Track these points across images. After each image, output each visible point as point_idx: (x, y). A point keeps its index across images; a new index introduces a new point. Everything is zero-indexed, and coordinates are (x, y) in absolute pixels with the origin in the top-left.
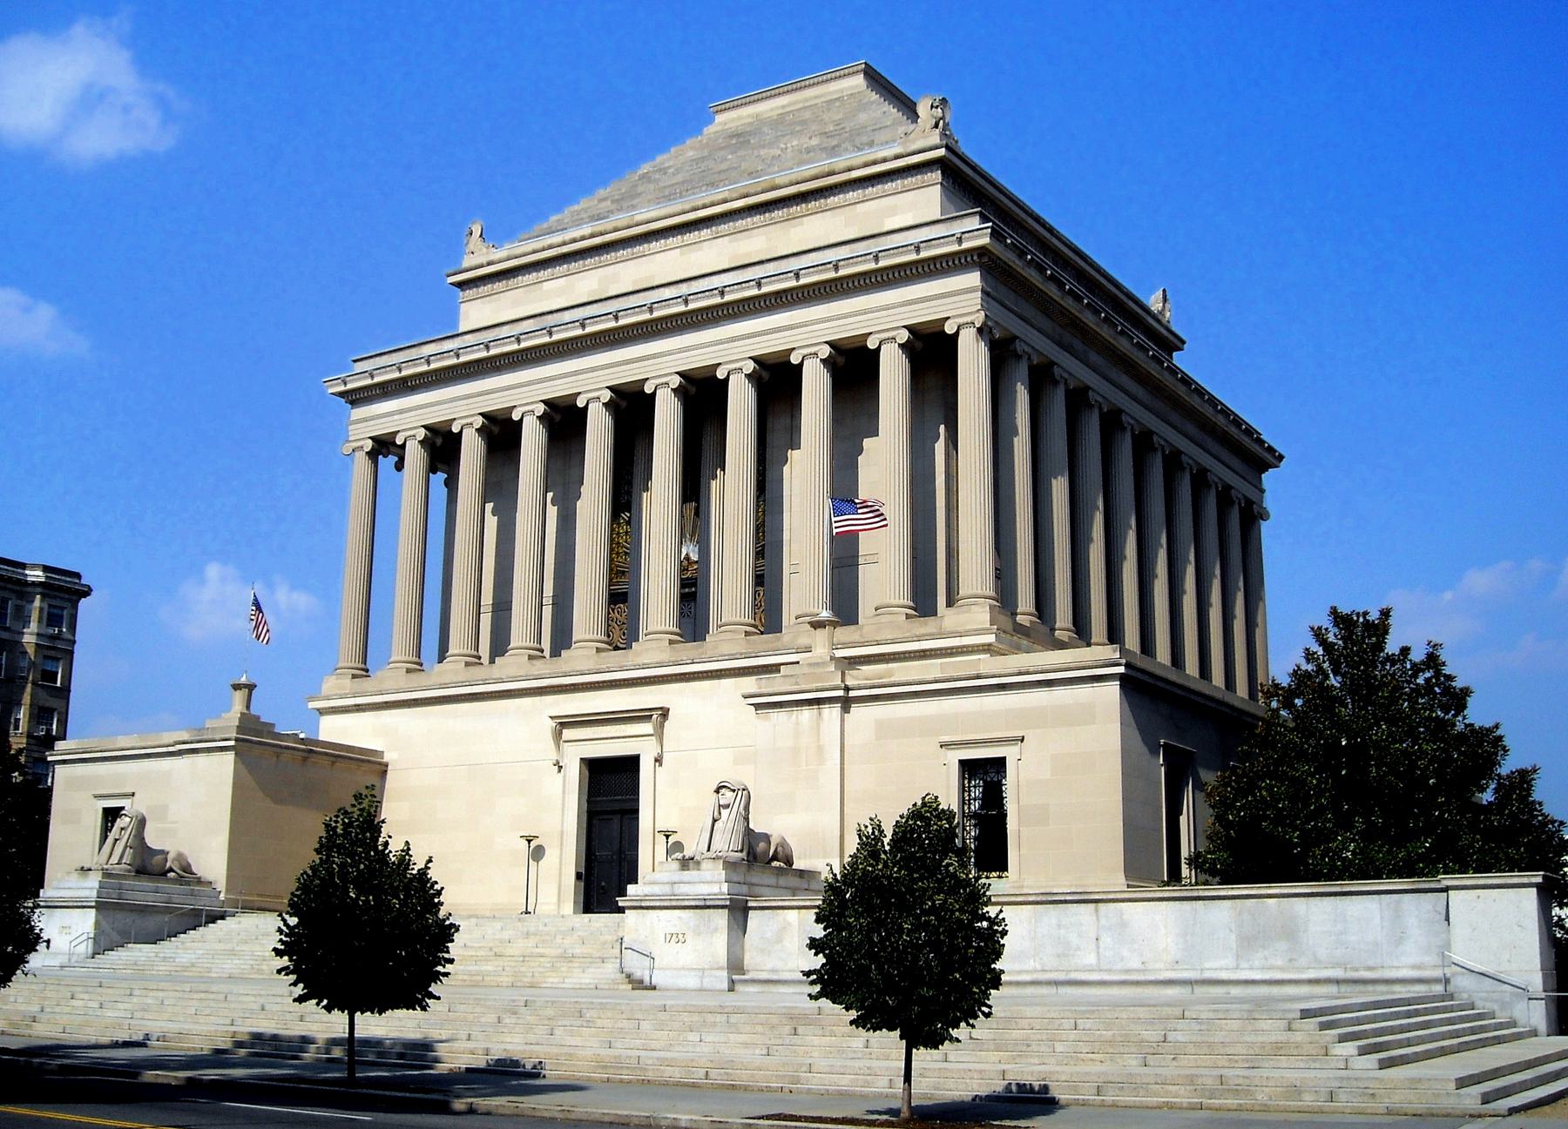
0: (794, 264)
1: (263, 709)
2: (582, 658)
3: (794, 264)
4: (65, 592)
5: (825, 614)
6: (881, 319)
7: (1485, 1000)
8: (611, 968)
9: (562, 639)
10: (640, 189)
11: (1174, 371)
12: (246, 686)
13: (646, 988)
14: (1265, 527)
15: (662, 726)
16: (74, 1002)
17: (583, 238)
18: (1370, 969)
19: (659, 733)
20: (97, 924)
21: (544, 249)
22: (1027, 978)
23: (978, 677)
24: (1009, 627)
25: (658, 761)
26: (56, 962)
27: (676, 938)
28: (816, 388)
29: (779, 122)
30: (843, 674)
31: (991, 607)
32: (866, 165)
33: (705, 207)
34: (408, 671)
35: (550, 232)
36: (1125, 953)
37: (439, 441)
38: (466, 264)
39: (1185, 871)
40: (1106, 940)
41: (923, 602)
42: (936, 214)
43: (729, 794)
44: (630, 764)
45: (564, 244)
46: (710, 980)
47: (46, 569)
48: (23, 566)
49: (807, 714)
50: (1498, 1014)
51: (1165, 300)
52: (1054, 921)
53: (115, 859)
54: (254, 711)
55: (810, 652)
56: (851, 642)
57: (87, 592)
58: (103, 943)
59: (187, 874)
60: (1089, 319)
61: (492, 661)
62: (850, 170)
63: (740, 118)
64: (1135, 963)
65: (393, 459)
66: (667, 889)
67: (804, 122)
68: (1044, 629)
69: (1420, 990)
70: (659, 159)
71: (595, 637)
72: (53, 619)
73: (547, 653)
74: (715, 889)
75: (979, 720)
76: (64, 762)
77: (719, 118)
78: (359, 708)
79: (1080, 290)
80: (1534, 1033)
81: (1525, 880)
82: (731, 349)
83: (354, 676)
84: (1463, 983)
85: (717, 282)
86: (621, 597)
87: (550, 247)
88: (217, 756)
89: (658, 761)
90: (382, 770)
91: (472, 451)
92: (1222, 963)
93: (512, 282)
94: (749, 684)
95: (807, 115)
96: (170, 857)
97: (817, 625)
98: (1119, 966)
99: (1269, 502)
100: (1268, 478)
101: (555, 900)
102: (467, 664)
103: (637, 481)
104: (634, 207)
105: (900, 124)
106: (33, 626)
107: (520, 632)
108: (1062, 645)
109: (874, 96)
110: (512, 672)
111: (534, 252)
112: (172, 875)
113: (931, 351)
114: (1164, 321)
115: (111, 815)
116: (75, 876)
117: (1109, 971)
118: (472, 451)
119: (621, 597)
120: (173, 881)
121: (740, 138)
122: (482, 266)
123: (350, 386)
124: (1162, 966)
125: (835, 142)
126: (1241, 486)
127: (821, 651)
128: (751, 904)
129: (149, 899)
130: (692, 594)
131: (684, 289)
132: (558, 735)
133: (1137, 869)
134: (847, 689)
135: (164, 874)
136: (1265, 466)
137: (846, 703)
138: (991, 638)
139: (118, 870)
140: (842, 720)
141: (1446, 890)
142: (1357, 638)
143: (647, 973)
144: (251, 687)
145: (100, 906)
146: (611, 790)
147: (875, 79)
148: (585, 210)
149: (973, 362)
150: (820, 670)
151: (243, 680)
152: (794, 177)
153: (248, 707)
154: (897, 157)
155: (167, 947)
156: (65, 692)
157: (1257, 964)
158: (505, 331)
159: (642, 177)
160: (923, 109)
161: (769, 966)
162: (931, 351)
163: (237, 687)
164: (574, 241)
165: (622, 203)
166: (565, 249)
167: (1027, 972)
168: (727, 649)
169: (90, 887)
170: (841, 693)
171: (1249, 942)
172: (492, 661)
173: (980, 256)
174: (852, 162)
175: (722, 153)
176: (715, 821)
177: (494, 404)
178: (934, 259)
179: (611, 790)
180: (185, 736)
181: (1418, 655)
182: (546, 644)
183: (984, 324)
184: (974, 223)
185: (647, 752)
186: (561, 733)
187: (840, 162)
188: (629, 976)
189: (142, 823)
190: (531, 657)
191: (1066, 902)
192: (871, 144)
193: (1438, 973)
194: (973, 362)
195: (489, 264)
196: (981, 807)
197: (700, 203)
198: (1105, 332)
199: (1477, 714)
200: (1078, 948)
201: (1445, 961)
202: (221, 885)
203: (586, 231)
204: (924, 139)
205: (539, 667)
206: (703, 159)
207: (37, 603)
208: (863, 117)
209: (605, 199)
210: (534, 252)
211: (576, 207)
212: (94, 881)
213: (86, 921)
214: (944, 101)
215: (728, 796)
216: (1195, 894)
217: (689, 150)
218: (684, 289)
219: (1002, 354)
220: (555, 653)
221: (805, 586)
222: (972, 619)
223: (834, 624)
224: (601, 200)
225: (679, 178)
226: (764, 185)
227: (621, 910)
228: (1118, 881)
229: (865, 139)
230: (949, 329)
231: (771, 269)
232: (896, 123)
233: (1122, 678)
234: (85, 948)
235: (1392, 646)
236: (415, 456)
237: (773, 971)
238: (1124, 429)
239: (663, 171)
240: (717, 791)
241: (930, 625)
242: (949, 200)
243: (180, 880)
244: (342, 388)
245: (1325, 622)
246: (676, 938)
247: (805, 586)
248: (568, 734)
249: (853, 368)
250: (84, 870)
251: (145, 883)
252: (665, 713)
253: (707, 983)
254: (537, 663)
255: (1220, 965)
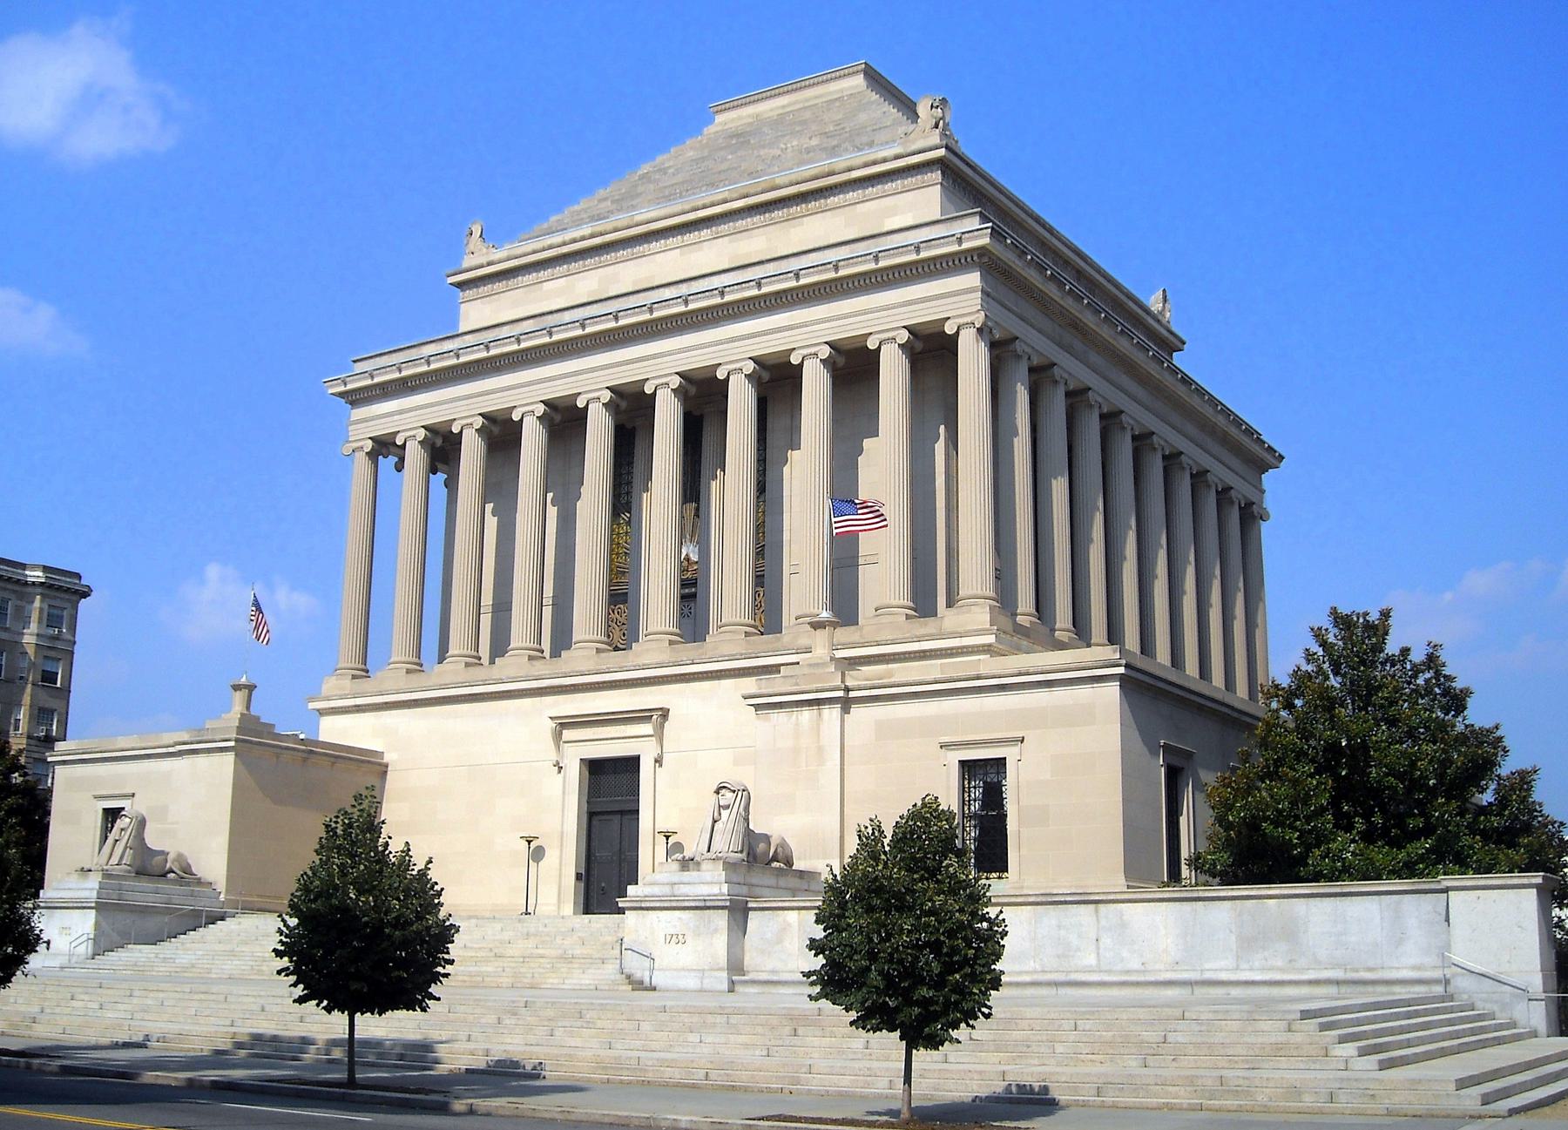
0: (795, 264)
1: (264, 710)
2: (582, 658)
3: (795, 264)
4: (66, 591)
5: (825, 615)
6: (880, 319)
7: (1485, 1001)
8: (611, 969)
9: (562, 640)
10: (640, 189)
11: (1174, 371)
12: (246, 687)
13: (646, 989)
14: (1265, 528)
15: (662, 727)
16: (74, 1003)
17: (583, 239)
18: (1370, 969)
19: (659, 734)
20: (97, 925)
21: (544, 250)
22: (1027, 978)
23: (978, 678)
24: (1010, 628)
25: (658, 761)
26: (56, 963)
27: (676, 938)
28: (815, 387)
29: (779, 121)
30: (843, 675)
31: (991, 607)
32: (866, 165)
33: (705, 207)
34: (408, 671)
35: (550, 232)
36: (1125, 954)
37: (439, 442)
38: (466, 264)
39: (1185, 871)
40: (1106, 941)
41: (923, 602)
42: (939, 217)
43: (730, 795)
44: (630, 765)
45: (564, 244)
46: (714, 980)
47: (46, 569)
48: (23, 566)
49: (806, 715)
50: (1498, 1015)
51: (1165, 300)
52: (1054, 922)
53: (115, 860)
54: (253, 711)
55: (811, 653)
56: (852, 644)
57: (85, 595)
58: (103, 944)
59: (186, 875)
60: (1089, 319)
61: (492, 662)
62: (850, 170)
63: (740, 118)
64: (1135, 964)
65: (393, 460)
66: (667, 890)
67: (804, 123)
68: (1044, 630)
69: (1420, 990)
70: (659, 159)
71: (595, 637)
72: (53, 620)
73: (547, 654)
74: (716, 890)
75: (979, 720)
76: (64, 762)
77: (719, 118)
78: (359, 709)
79: (1081, 289)
80: (1534, 1034)
81: (1525, 881)
82: (731, 350)
83: (354, 677)
84: (1463, 984)
85: (717, 282)
86: (621, 596)
87: (551, 247)
88: (216, 757)
89: (658, 761)
90: (383, 771)
91: (472, 451)
92: (1222, 964)
93: (512, 283)
94: (749, 684)
95: (808, 115)
96: (170, 857)
97: (817, 626)
98: (1119, 967)
99: (1269, 502)
100: (1267, 478)
101: (554, 900)
102: (467, 665)
103: (637, 482)
104: (634, 208)
105: (900, 124)
106: (34, 627)
107: (520, 633)
108: (1061, 646)
109: (874, 97)
110: (512, 673)
111: (534, 252)
112: (172, 875)
113: (931, 352)
114: (1164, 321)
115: (112, 815)
116: (75, 876)
117: (1109, 972)
118: (472, 451)
119: (621, 596)
120: (173, 881)
121: (740, 138)
122: (482, 266)
123: (349, 387)
124: (1162, 967)
125: (835, 143)
126: (1241, 489)
127: (821, 651)
128: (750, 905)
129: (150, 900)
130: (691, 592)
131: (684, 290)
132: (557, 736)
133: (1135, 870)
134: (847, 690)
135: (164, 875)
136: (1263, 467)
137: (846, 704)
138: (991, 639)
139: (117, 870)
140: (842, 721)
141: (1446, 890)
142: (1357, 641)
143: (647, 974)
144: (251, 688)
145: (100, 907)
146: (611, 789)
147: (875, 79)
148: (585, 210)
149: (973, 361)
150: (820, 671)
151: (244, 680)
152: (793, 178)
153: (248, 708)
154: (897, 157)
155: (167, 948)
156: (66, 690)
157: (1257, 964)
158: (505, 332)
159: (642, 177)
160: (923, 109)
161: (769, 967)
162: (931, 352)
163: (236, 688)
164: (574, 241)
165: (622, 203)
166: (565, 249)
167: (1027, 972)
168: (727, 649)
169: (89, 888)
170: (841, 694)
171: (1249, 943)
172: (492, 662)
173: (980, 256)
174: (851, 162)
175: (722, 153)
176: (715, 822)
177: (494, 404)
178: (934, 259)
179: (611, 789)
180: (186, 737)
181: (1417, 656)
182: (546, 645)
183: (984, 324)
184: (974, 223)
185: (647, 752)
186: (561, 734)
187: (840, 162)
188: (628, 977)
189: (142, 823)
190: (531, 658)
191: (1066, 903)
192: (871, 144)
193: (1437, 974)
194: (973, 361)
195: (489, 264)
196: (983, 808)
197: (700, 203)
198: (1105, 332)
199: (1477, 715)
200: (1078, 949)
201: (1445, 961)
202: (221, 886)
203: (586, 231)
204: (924, 140)
205: (539, 668)
206: (703, 159)
207: (37, 603)
208: (863, 117)
209: (605, 199)
210: (534, 252)
211: (576, 207)
212: (94, 882)
213: (85, 923)
214: (944, 101)
215: (728, 797)
216: (1195, 895)
217: (689, 150)
218: (684, 290)
219: (1000, 351)
220: (555, 653)
221: (804, 588)
222: (972, 619)
223: (834, 625)
224: (600, 201)
225: (679, 178)
226: (764, 186)
227: (621, 911)
228: (1119, 882)
229: (865, 139)
230: (949, 329)
231: (771, 269)
232: (896, 123)
233: (1122, 679)
234: (85, 949)
235: (1392, 647)
236: (415, 456)
237: (773, 972)
238: (1232, 503)
239: (664, 171)
240: (717, 792)
241: (930, 625)
242: (950, 200)
243: (180, 880)
244: (342, 389)
245: (1325, 622)
246: (676, 938)
247: (804, 588)
248: (568, 734)
249: (853, 368)
250: (85, 871)
251: (145, 884)
252: (665, 714)
253: (707, 984)
254: (537, 663)
255: (1220, 966)
